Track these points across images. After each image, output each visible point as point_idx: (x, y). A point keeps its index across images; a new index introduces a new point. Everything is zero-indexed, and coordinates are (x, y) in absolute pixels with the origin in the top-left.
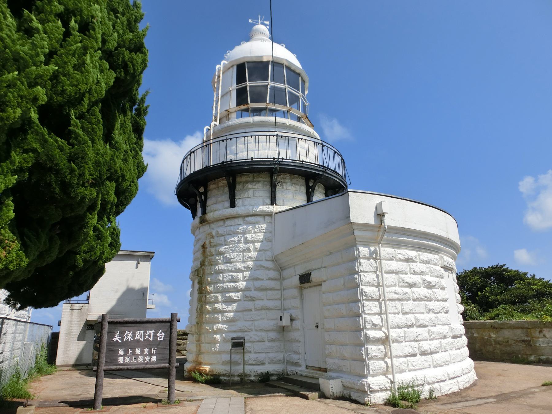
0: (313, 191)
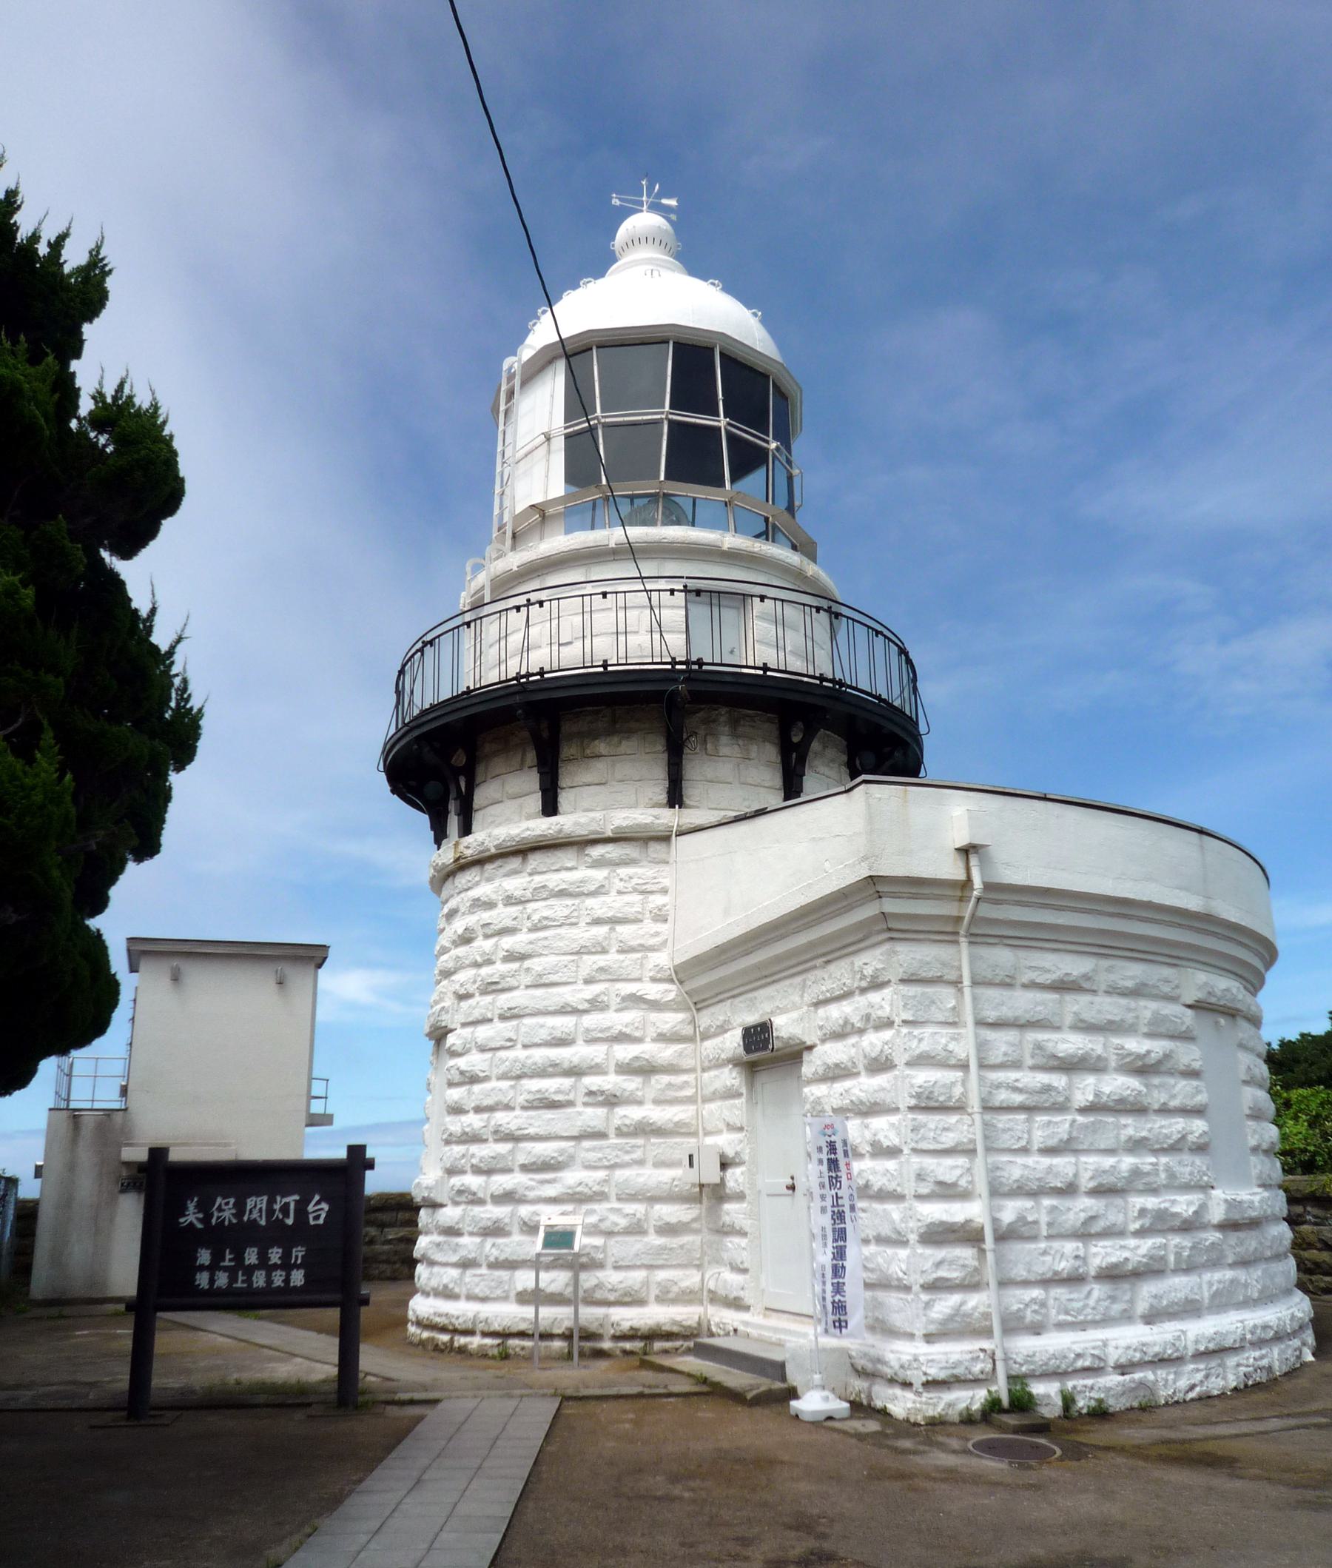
0: (802, 760)
